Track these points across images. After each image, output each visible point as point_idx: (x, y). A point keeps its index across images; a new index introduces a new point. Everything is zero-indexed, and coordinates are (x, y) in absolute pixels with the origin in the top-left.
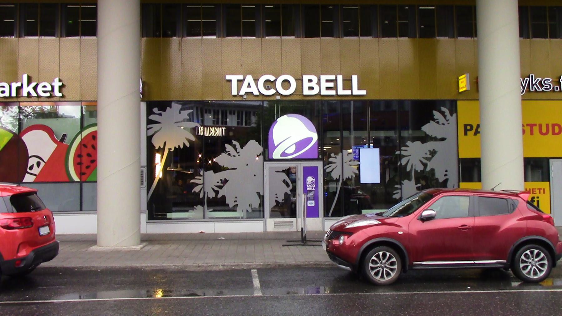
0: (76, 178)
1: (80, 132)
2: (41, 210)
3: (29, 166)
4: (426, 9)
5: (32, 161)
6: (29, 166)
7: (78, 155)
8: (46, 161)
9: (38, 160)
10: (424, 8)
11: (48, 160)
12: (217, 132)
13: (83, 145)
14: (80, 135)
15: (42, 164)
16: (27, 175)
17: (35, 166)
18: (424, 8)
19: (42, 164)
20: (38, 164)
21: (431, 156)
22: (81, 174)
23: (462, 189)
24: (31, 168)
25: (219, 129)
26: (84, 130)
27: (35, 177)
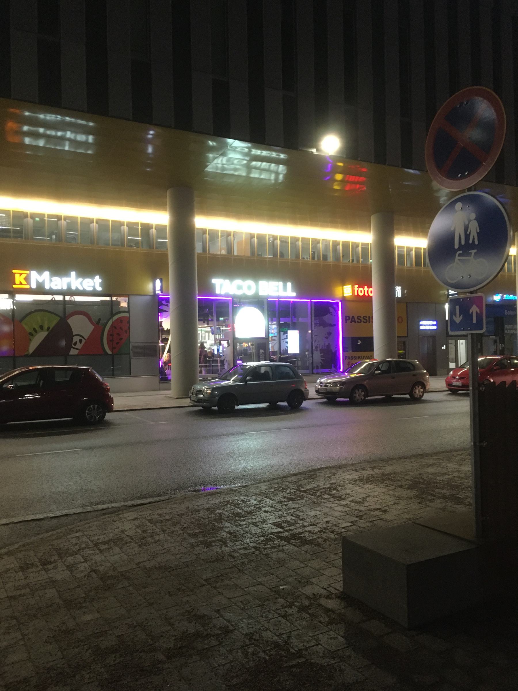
0: (109, 352)
1: (111, 318)
2: (327, 258)
3: (73, 342)
4: (52, 421)
5: (76, 339)
6: (73, 342)
7: (110, 335)
8: (86, 338)
9: (80, 338)
10: (59, 419)
11: (88, 338)
12: (220, 632)
13: (113, 327)
14: (111, 320)
15: (84, 341)
16: (72, 349)
17: (78, 342)
18: (59, 419)
19: (84, 341)
20: (81, 341)
21: (328, 336)
22: (112, 349)
23: (443, 378)
24: (75, 344)
25: (433, 325)
26: (113, 316)
27: (78, 351)
